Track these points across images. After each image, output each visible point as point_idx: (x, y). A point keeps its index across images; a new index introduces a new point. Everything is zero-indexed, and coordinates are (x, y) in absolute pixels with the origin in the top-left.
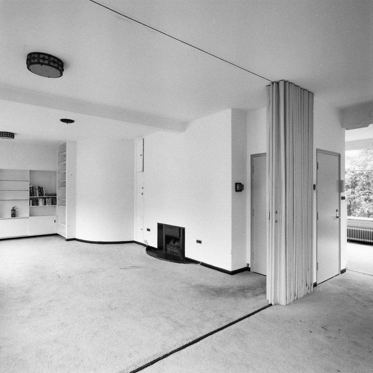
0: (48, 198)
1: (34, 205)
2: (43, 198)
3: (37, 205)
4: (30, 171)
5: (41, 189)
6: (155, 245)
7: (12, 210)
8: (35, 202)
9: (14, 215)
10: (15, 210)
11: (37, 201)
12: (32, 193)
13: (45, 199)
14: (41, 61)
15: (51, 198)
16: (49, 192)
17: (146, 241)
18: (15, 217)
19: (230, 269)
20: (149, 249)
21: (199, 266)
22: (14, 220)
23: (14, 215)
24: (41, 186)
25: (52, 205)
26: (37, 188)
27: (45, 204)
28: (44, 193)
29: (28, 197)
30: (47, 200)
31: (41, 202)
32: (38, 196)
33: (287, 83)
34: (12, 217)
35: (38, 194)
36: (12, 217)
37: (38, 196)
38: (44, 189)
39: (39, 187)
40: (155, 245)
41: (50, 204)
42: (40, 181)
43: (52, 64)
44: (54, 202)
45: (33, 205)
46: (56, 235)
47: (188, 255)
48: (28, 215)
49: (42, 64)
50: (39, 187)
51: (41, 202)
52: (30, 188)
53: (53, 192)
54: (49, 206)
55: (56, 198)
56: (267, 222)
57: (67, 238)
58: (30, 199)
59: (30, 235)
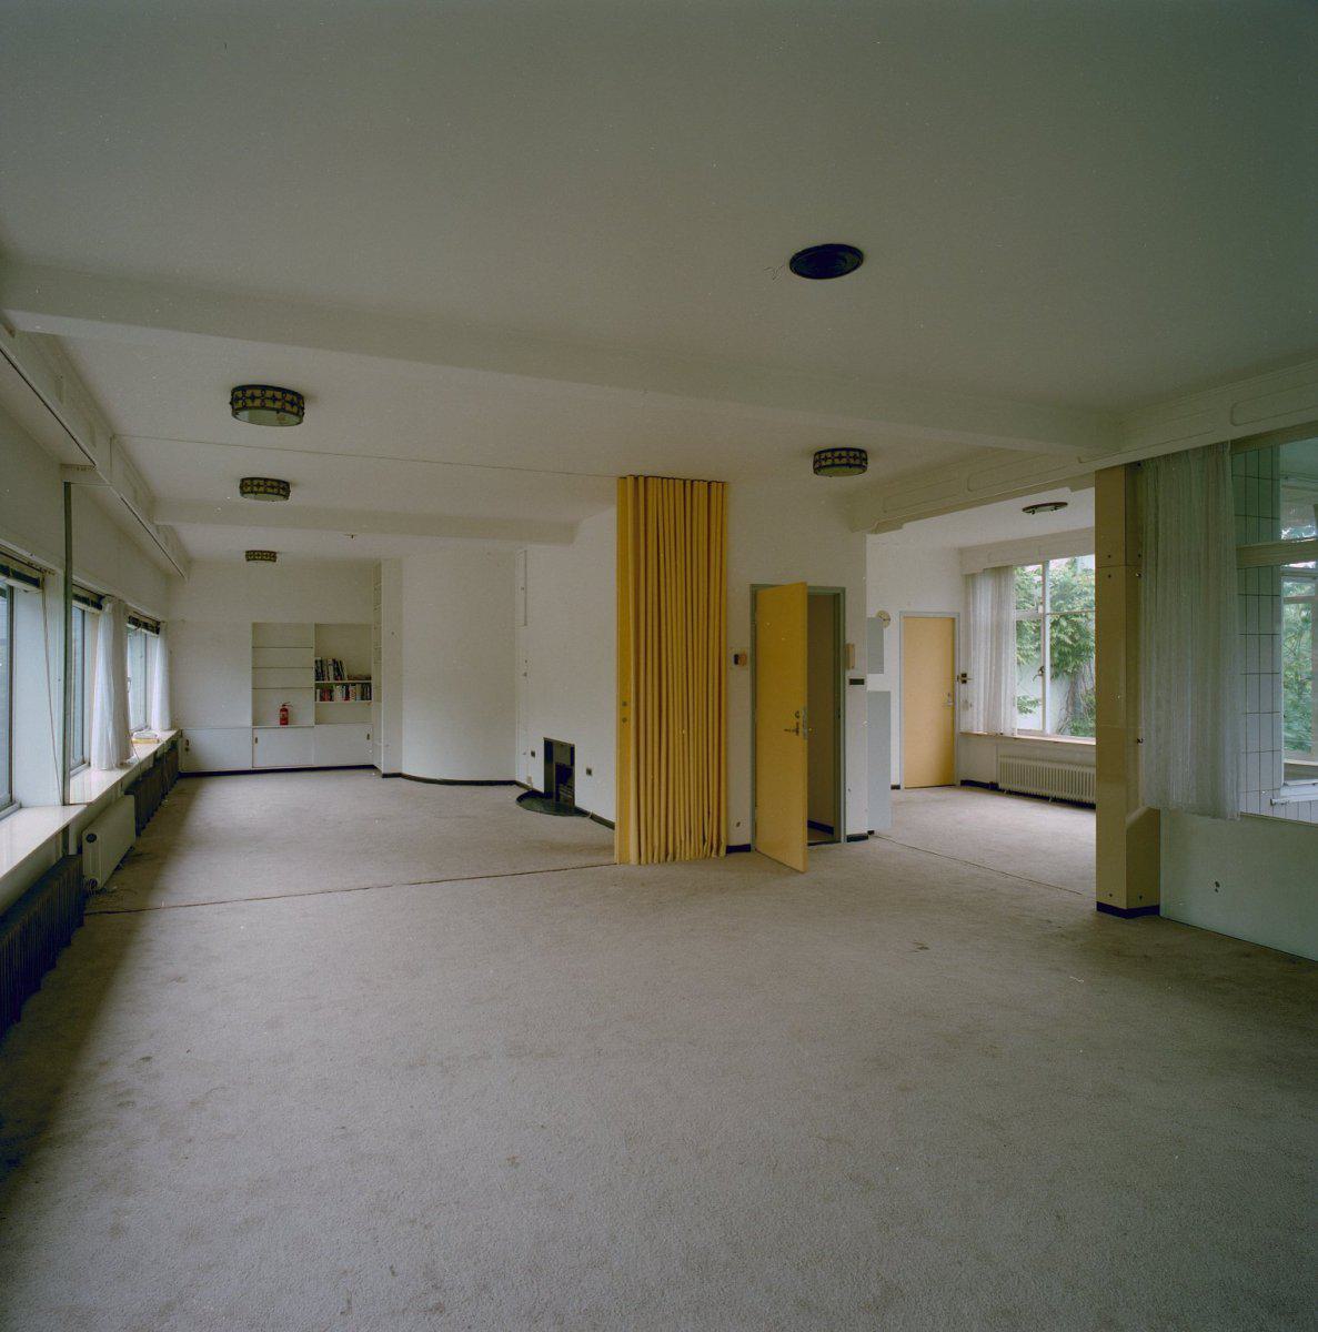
0: (354, 685)
1: (324, 700)
2: (344, 684)
3: (331, 699)
4: (316, 625)
5: (338, 666)
6: (539, 786)
7: (282, 710)
8: (325, 694)
9: (284, 721)
10: (286, 710)
11: (331, 691)
12: (320, 675)
13: (347, 686)
14: (255, 489)
15: (359, 687)
16: (357, 672)
17: (529, 779)
18: (287, 724)
19: (1122, 905)
20: (529, 796)
21: (587, 820)
22: (286, 732)
23: (284, 721)
24: (338, 659)
25: (362, 699)
26: (331, 661)
27: (347, 698)
28: (346, 674)
29: (312, 682)
30: (351, 688)
31: (338, 693)
32: (332, 681)
33: (714, 485)
34: (281, 724)
35: (332, 677)
36: (281, 724)
37: (332, 681)
38: (344, 666)
39: (334, 660)
40: (539, 786)
41: (358, 697)
42: (337, 648)
43: (269, 490)
44: (366, 693)
45: (322, 699)
46: (372, 767)
47: (579, 803)
48: (311, 721)
49: (256, 493)
50: (334, 660)
51: (338, 693)
52: (316, 662)
53: (365, 673)
54: (354, 702)
55: (369, 685)
56: (892, 743)
57: (384, 771)
58: (317, 686)
59: (316, 766)
